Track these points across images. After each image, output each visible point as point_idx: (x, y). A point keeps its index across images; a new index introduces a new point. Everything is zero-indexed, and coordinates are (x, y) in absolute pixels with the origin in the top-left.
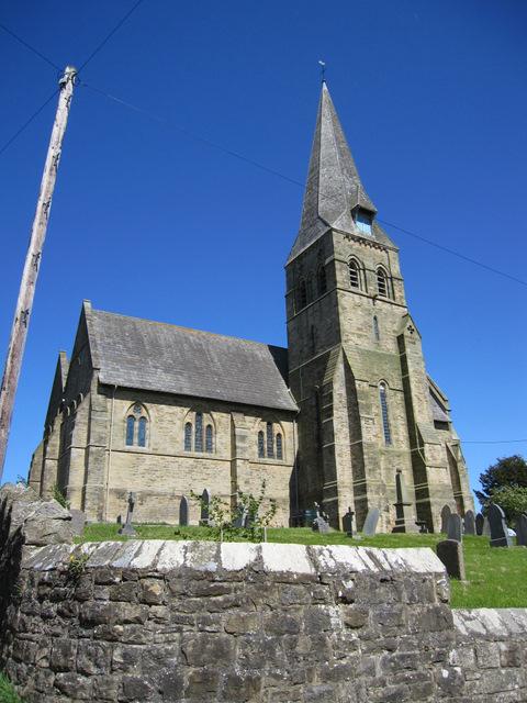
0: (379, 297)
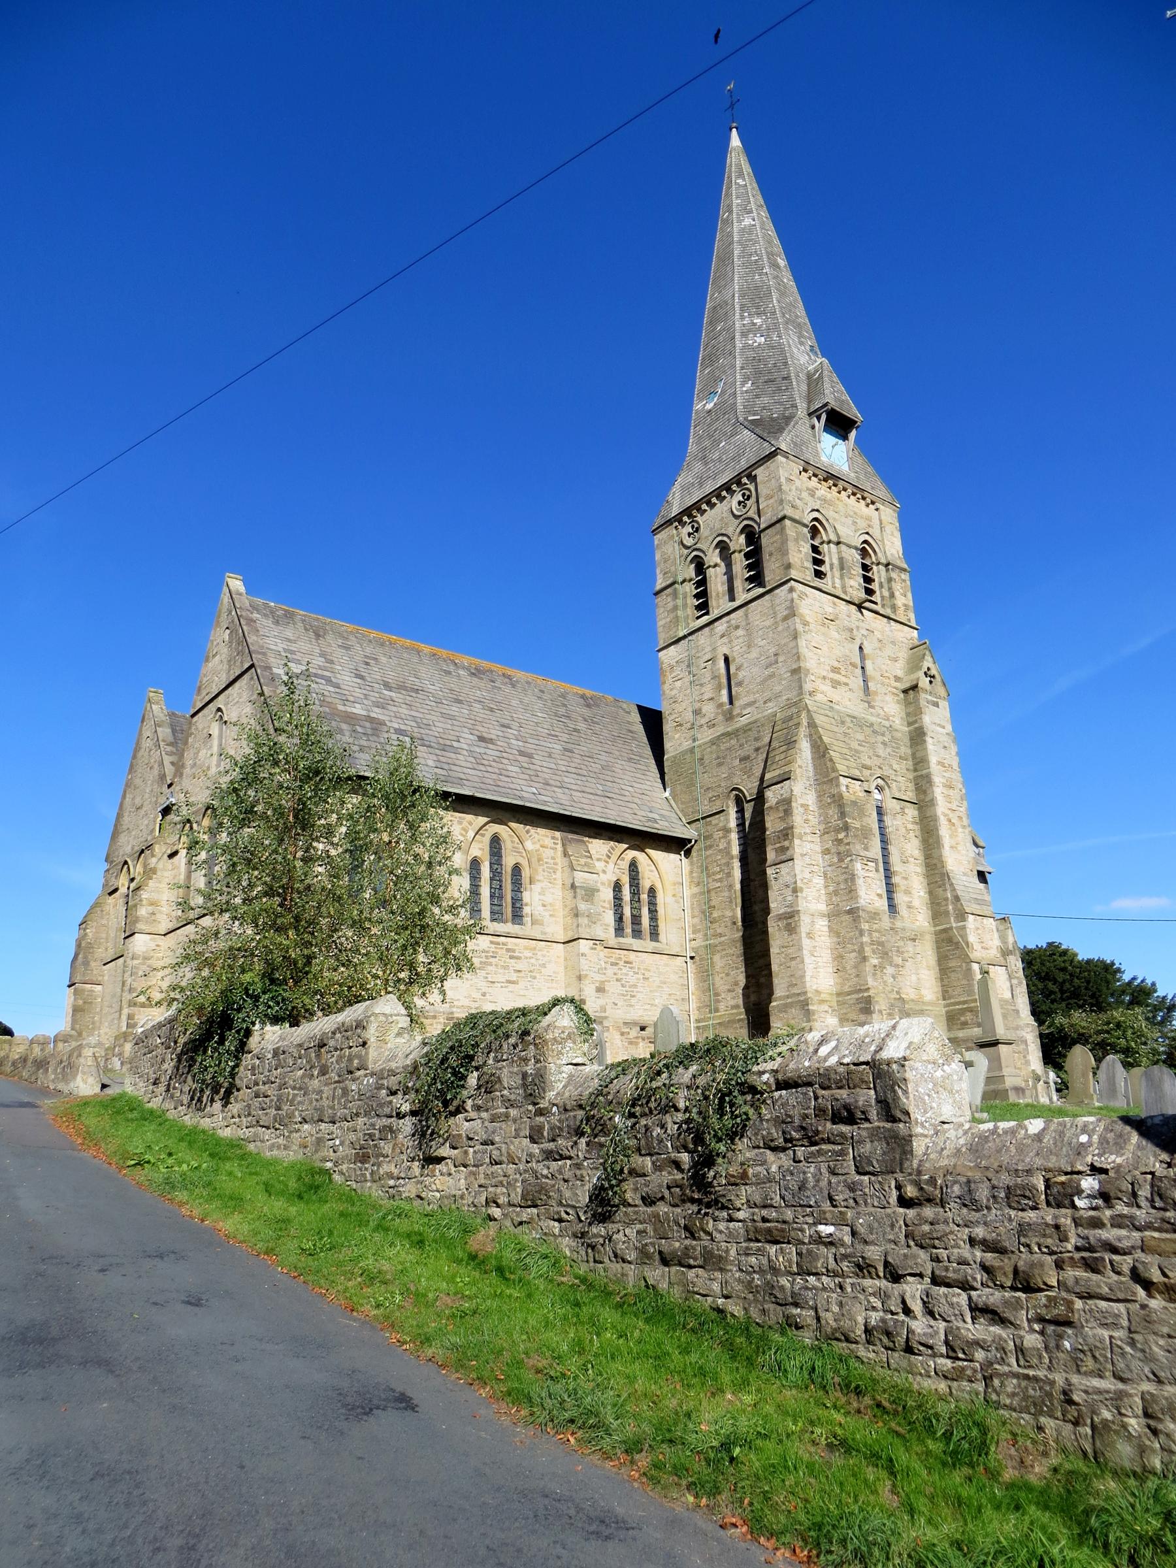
0: (867, 604)
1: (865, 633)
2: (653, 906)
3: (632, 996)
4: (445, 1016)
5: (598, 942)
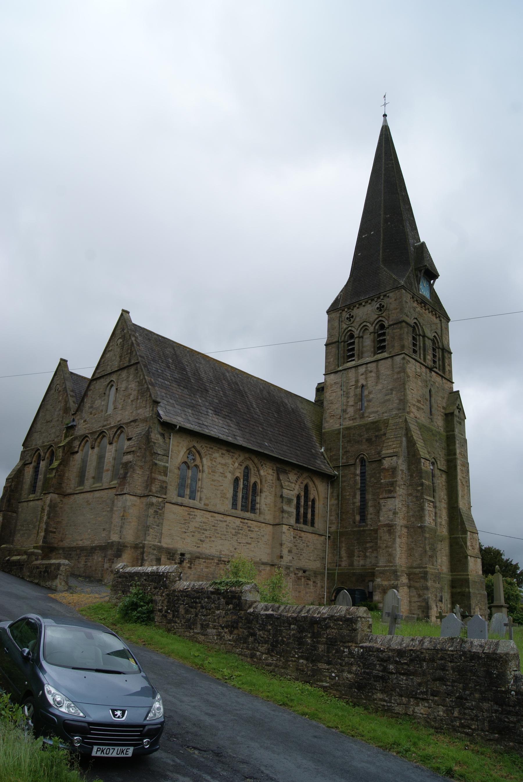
1: (432, 383)
2: (313, 507)
3: (301, 555)
4: (218, 559)
5: (291, 527)
